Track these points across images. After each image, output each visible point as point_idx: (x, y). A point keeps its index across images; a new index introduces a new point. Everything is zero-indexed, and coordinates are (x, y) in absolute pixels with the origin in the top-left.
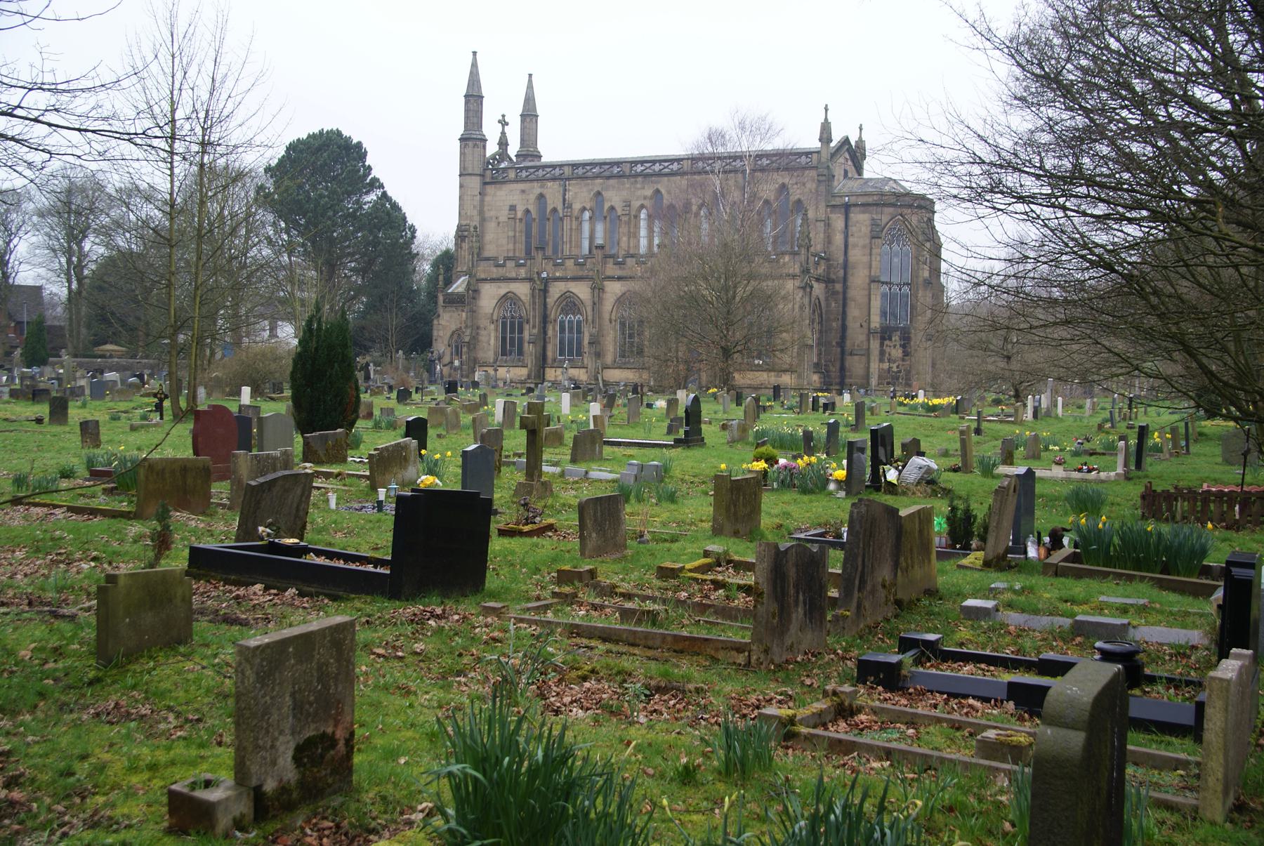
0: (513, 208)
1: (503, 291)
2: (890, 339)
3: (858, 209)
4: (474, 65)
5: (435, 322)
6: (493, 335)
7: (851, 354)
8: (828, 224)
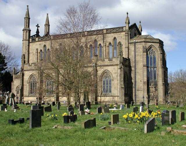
0: (37, 49)
1: (31, 74)
5: (12, 84)
6: (28, 87)
7: (138, 90)
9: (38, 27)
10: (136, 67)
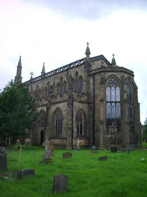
2: (111, 125)
3: (97, 75)
4: (20, 59)
8: (88, 82)
9: (32, 75)
10: (95, 104)
